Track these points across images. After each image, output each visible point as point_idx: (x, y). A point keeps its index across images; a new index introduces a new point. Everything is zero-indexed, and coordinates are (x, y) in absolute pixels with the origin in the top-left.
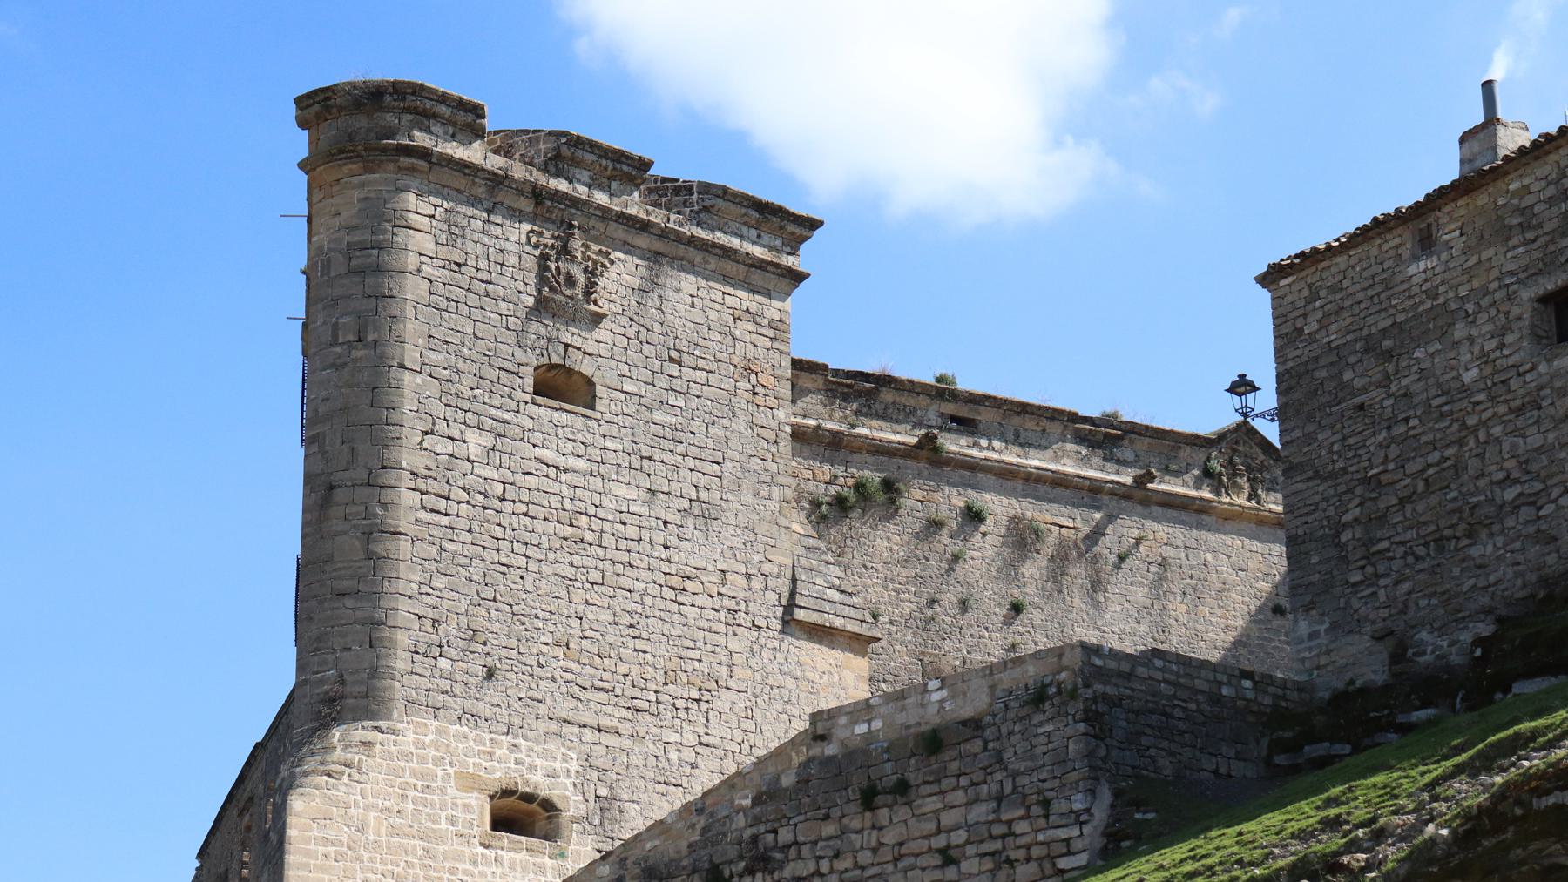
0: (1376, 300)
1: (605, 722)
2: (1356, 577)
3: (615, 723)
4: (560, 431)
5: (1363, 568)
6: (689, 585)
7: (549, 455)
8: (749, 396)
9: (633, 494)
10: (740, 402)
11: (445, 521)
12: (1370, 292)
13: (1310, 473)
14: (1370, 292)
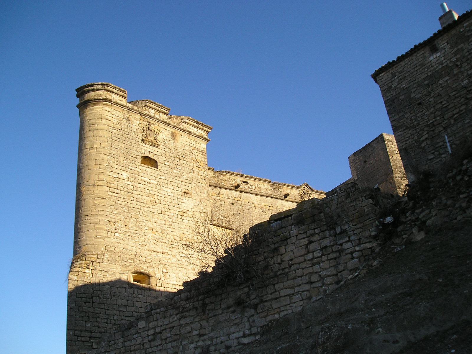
0: (418, 71)
1: (164, 251)
2: (432, 156)
3: (167, 251)
4: (148, 173)
5: (433, 153)
6: (185, 214)
7: (146, 179)
8: (197, 168)
9: (169, 190)
10: (195, 169)
11: (116, 195)
12: (416, 69)
13: (404, 128)
14: (416, 69)
